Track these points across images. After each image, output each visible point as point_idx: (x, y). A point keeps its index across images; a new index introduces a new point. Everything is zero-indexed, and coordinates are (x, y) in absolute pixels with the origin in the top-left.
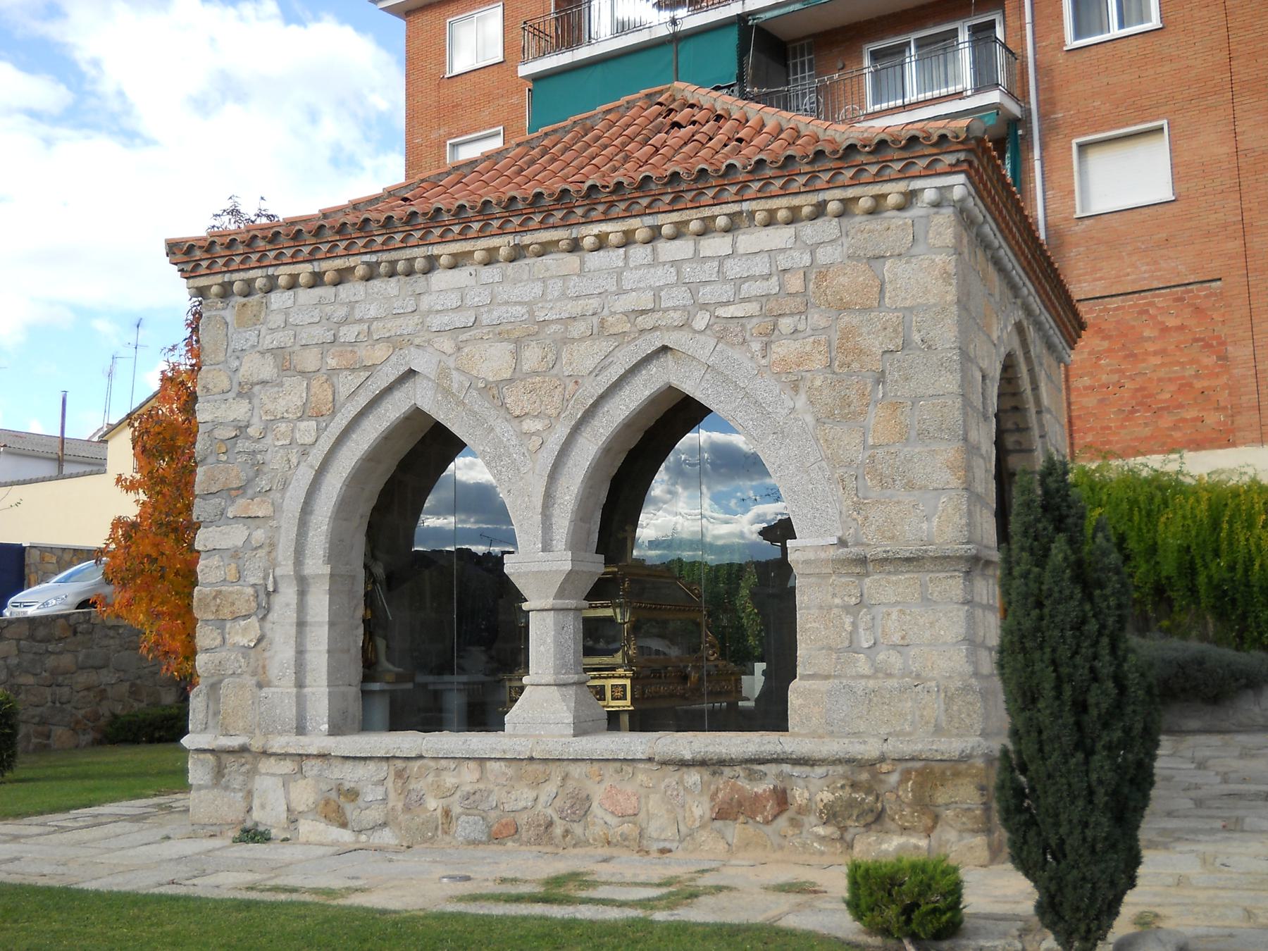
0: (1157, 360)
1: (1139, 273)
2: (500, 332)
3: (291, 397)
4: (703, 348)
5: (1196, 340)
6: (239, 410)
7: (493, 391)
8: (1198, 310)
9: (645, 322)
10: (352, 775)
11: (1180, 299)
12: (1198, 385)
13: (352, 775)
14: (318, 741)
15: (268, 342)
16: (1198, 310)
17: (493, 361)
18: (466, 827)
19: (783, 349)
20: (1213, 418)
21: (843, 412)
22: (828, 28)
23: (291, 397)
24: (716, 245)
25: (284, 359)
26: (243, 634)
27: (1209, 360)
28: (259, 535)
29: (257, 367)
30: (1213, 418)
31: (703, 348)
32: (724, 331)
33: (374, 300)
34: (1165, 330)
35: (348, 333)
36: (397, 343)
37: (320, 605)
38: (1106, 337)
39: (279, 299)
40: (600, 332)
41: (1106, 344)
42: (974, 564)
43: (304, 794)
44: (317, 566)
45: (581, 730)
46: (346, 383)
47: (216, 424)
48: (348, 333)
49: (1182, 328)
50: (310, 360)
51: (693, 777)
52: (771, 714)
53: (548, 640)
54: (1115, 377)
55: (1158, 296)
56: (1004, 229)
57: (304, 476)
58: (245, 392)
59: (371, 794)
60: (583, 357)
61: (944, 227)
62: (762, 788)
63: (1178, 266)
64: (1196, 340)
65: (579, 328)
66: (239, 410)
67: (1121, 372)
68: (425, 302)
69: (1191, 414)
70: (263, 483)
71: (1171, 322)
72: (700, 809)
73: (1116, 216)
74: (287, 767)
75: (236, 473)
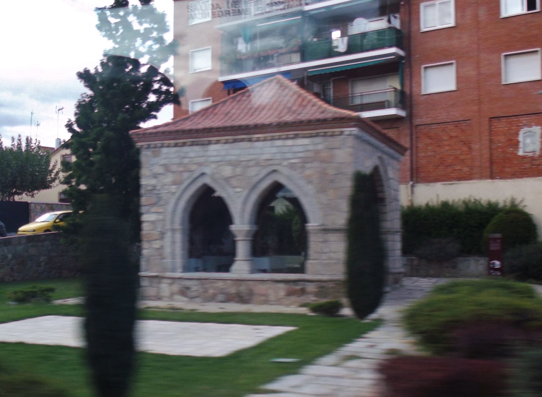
0: (447, 148)
1: (443, 116)
2: (230, 163)
3: (169, 179)
4: (285, 171)
5: (462, 141)
6: (153, 182)
7: (227, 179)
8: (463, 131)
9: (271, 162)
10: (188, 283)
11: (456, 126)
12: (462, 157)
13: (188, 283)
14: (178, 275)
15: (163, 162)
16: (463, 131)
17: (227, 171)
18: (221, 297)
19: (308, 172)
20: (466, 169)
21: (322, 190)
22: (281, 312)
23: (169, 179)
24: (289, 142)
25: (166, 167)
26: (156, 245)
27: (465, 149)
28: (161, 217)
29: (158, 169)
30: (466, 169)
31: (285, 171)
32: (292, 166)
33: (193, 152)
34: (451, 137)
35: (186, 161)
36: (200, 164)
37: (178, 237)
38: (431, 139)
39: (165, 150)
40: (257, 164)
41: (430, 141)
42: (412, 204)
43: (176, 288)
44: (177, 226)
45: (253, 272)
46: (186, 175)
47: (147, 185)
48: (186, 161)
49: (456, 137)
50: (174, 168)
51: (281, 285)
52: (301, 270)
53: (242, 249)
54: (433, 153)
55: (449, 125)
56: (372, 135)
57: (173, 201)
58: (155, 176)
59: (194, 288)
60: (253, 172)
61: (351, 142)
62: (298, 287)
63: (456, 114)
64: (462, 141)
65: (252, 163)
66: (153, 182)
67: (434, 151)
68: (209, 153)
69: (458, 167)
70: (161, 203)
71: (453, 134)
72: (282, 293)
73: (436, 95)
74: (169, 281)
75: (153, 200)
